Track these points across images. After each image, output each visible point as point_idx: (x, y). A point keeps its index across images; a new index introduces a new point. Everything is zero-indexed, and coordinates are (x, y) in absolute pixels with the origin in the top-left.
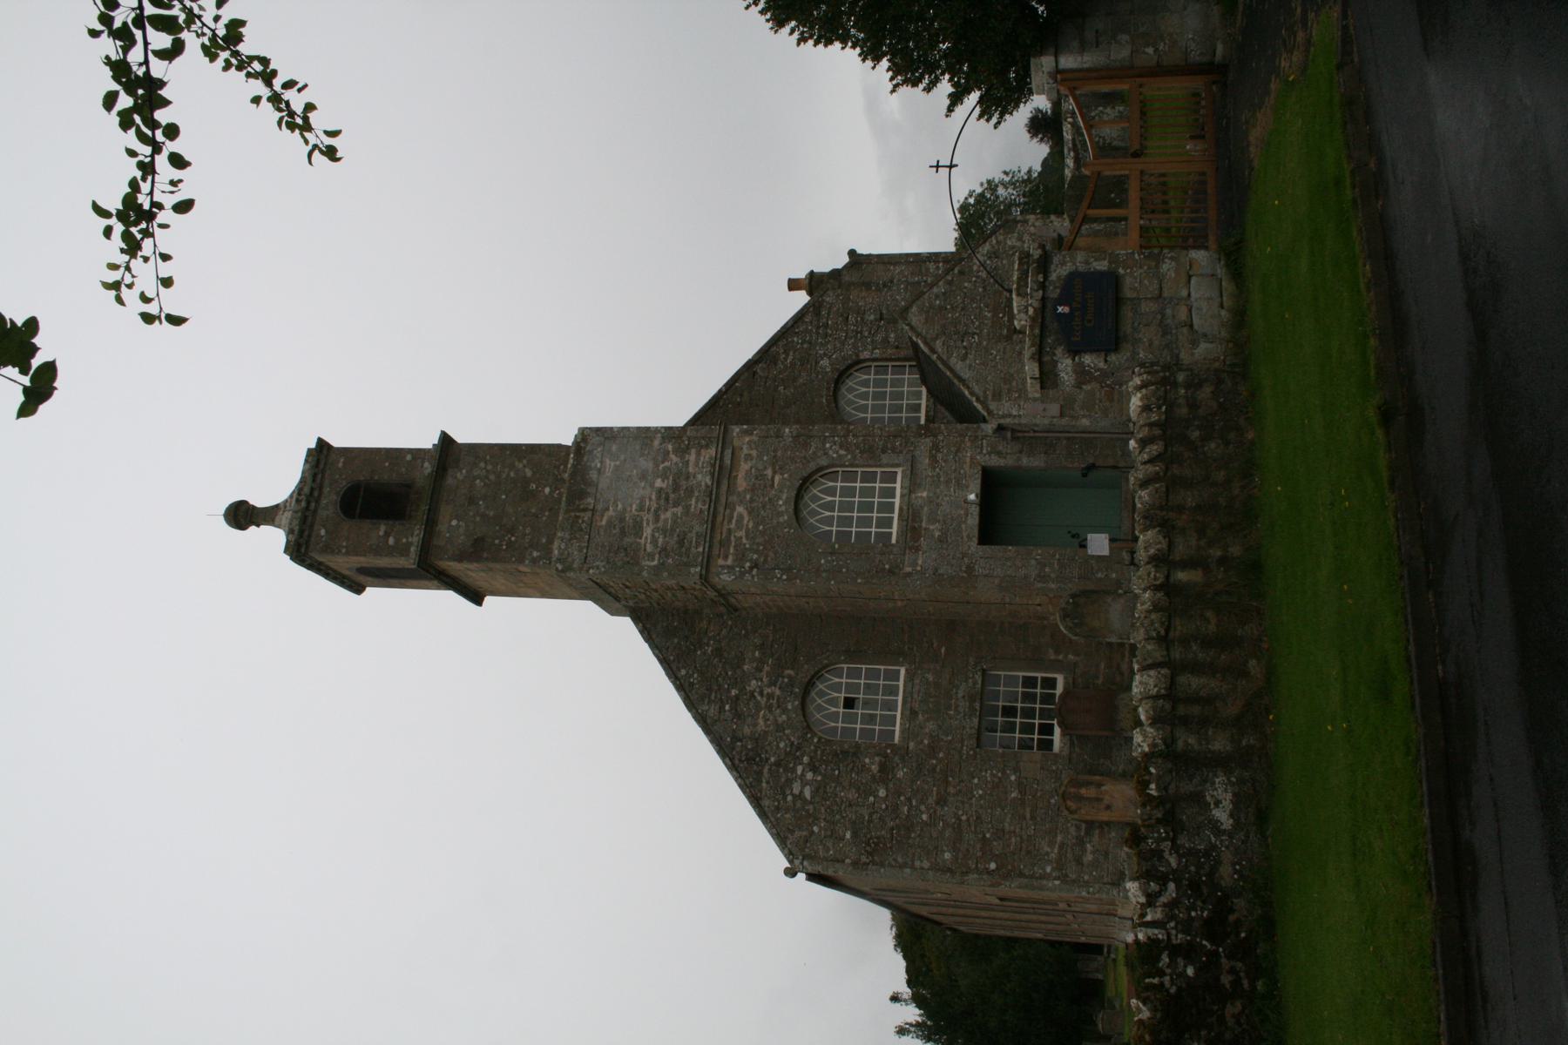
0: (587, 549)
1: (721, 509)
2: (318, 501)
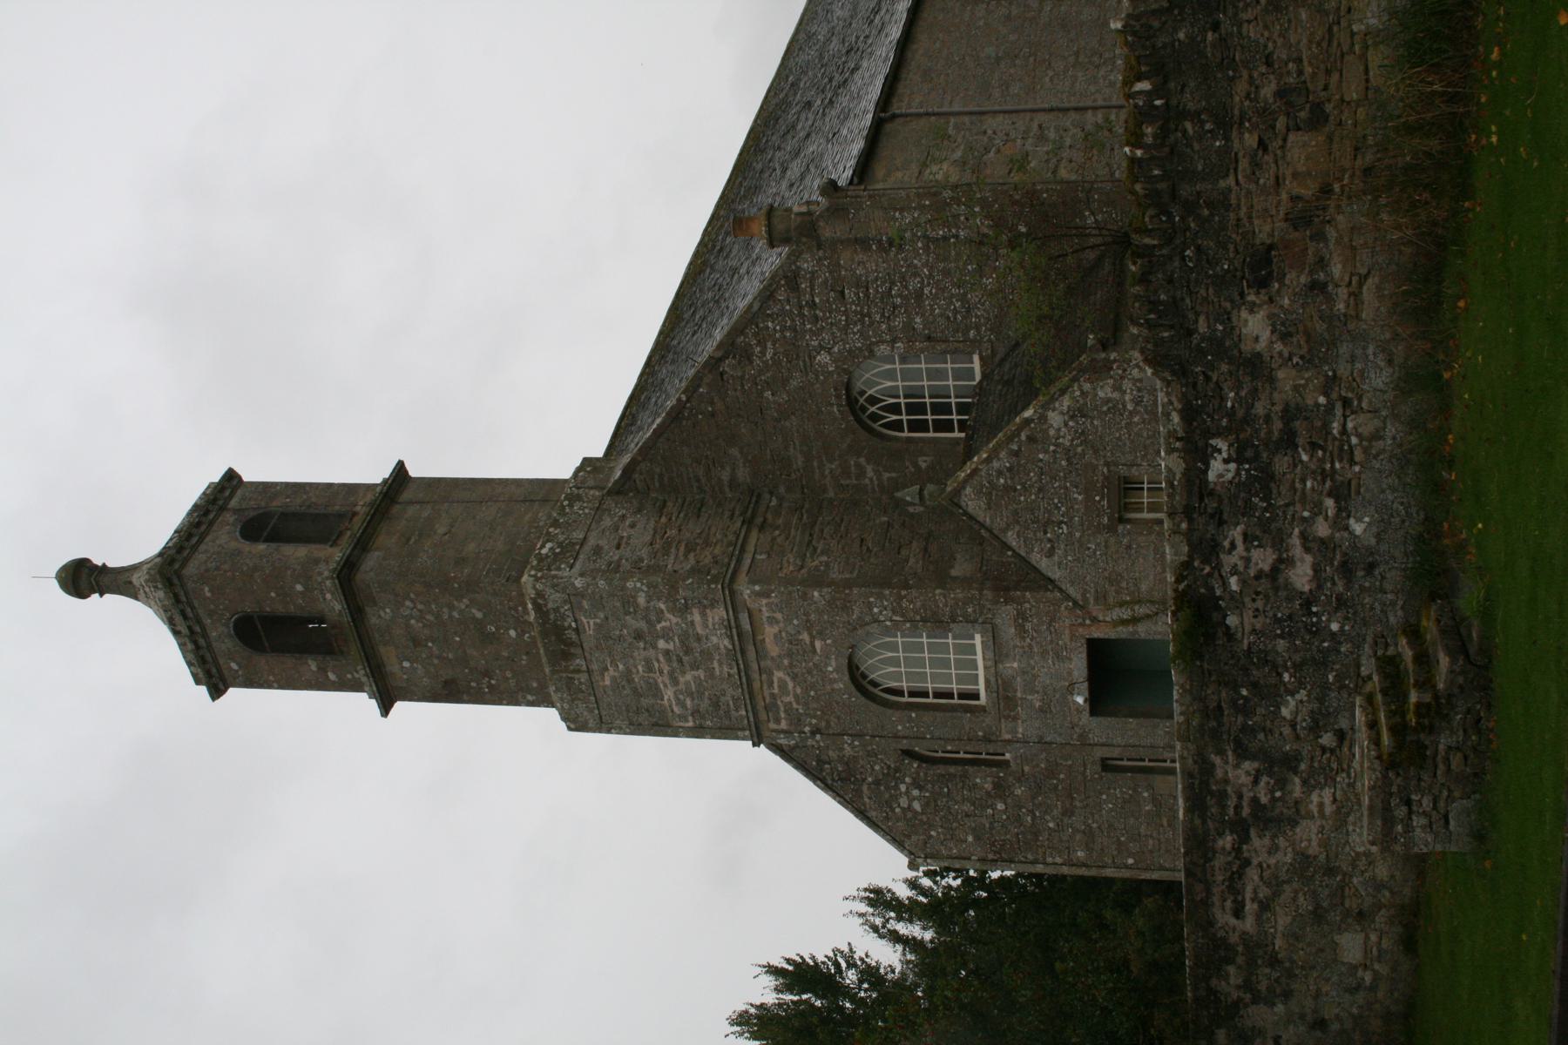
0: (598, 709)
1: (756, 676)
2: (205, 636)
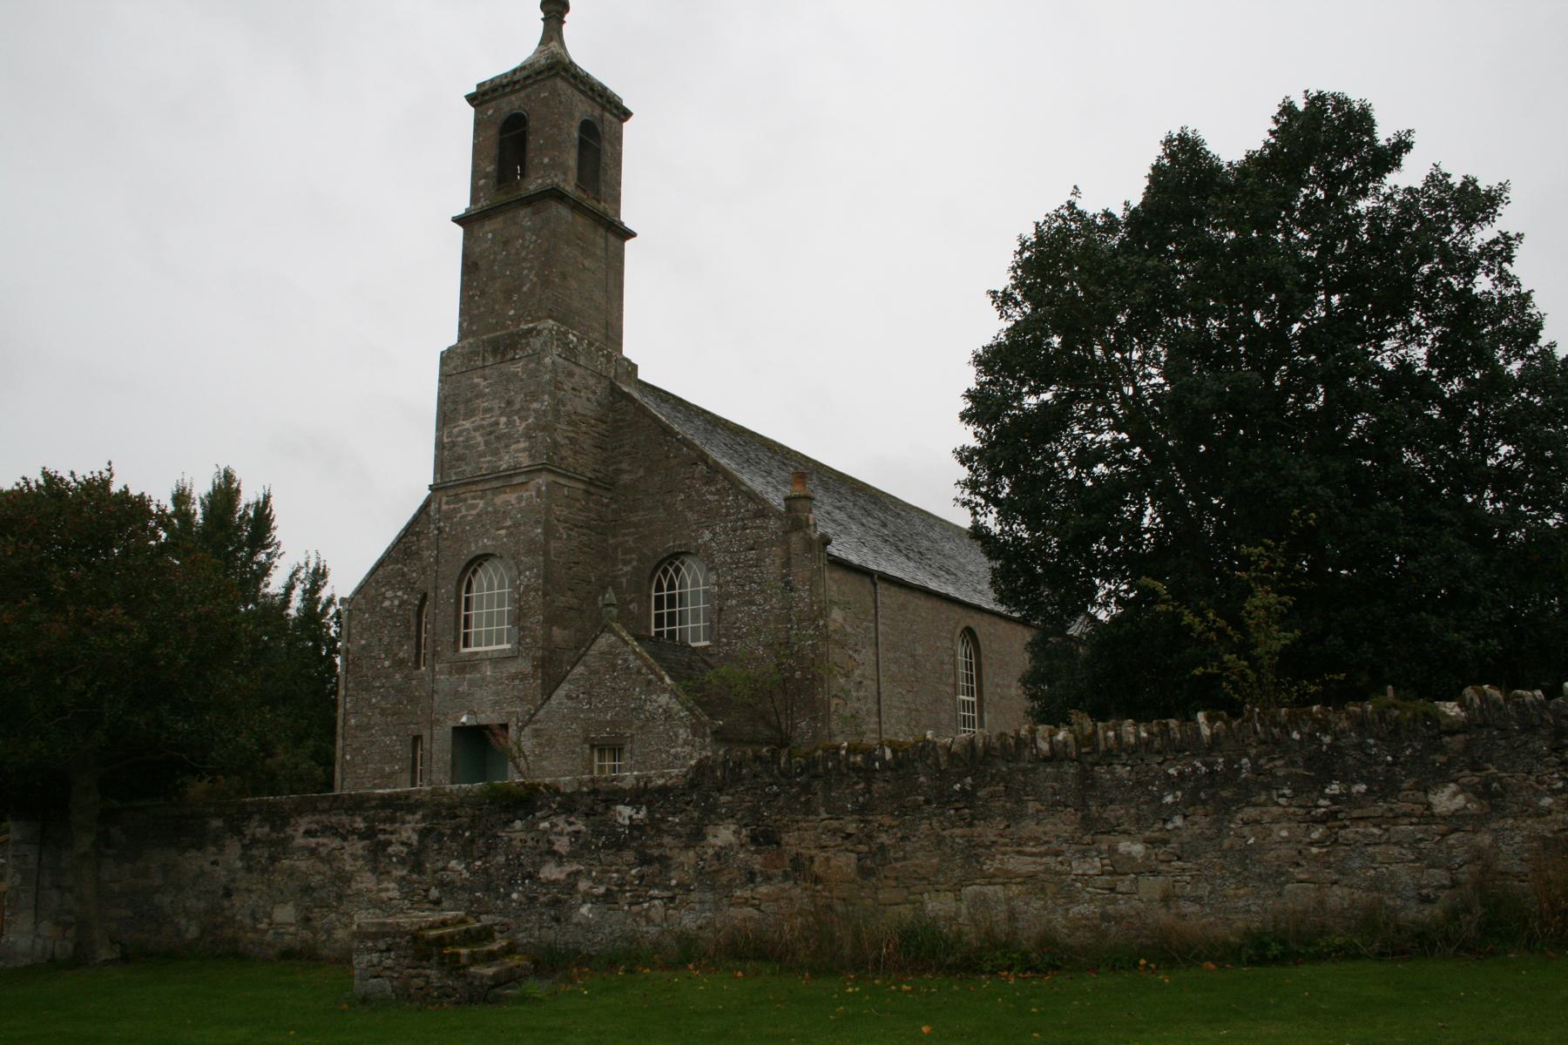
1: (480, 487)
2: (513, 92)
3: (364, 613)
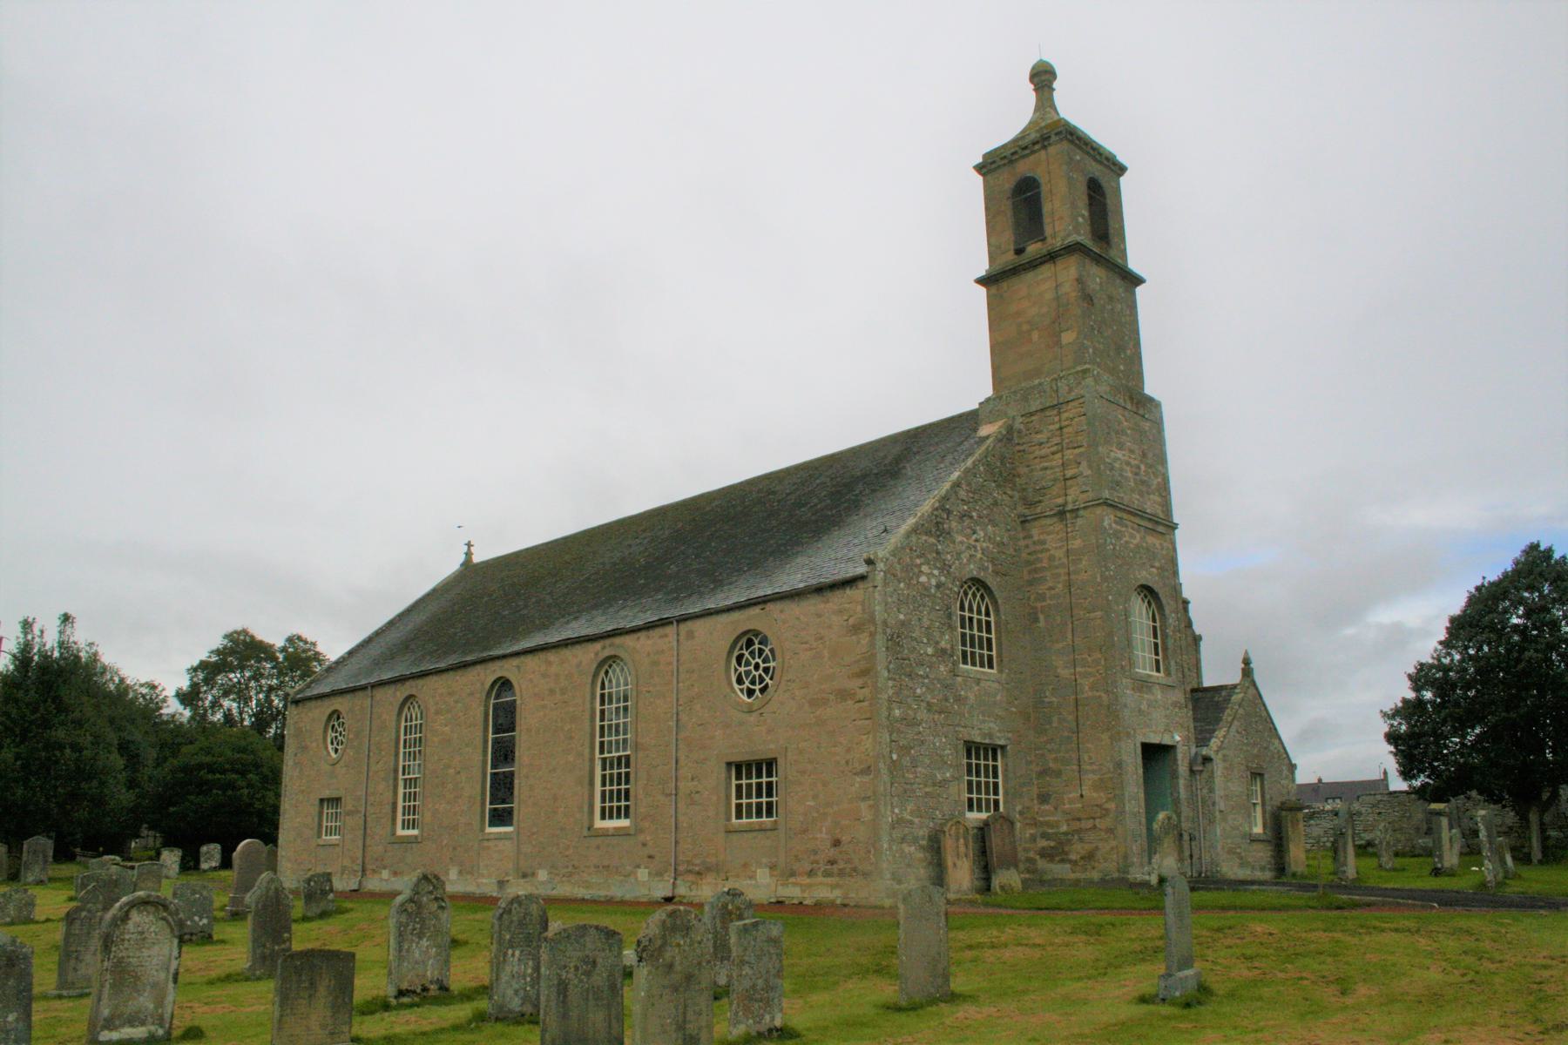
3: (900, 582)
